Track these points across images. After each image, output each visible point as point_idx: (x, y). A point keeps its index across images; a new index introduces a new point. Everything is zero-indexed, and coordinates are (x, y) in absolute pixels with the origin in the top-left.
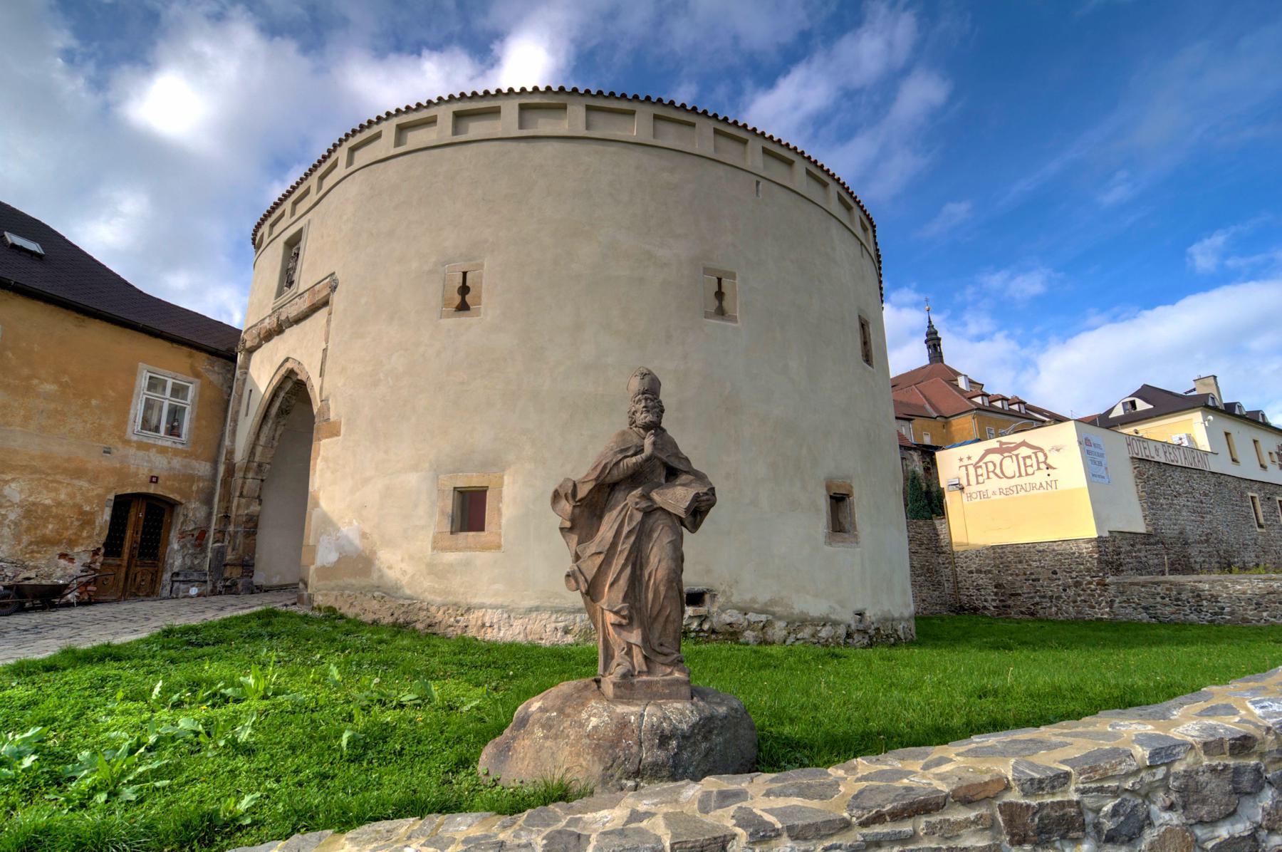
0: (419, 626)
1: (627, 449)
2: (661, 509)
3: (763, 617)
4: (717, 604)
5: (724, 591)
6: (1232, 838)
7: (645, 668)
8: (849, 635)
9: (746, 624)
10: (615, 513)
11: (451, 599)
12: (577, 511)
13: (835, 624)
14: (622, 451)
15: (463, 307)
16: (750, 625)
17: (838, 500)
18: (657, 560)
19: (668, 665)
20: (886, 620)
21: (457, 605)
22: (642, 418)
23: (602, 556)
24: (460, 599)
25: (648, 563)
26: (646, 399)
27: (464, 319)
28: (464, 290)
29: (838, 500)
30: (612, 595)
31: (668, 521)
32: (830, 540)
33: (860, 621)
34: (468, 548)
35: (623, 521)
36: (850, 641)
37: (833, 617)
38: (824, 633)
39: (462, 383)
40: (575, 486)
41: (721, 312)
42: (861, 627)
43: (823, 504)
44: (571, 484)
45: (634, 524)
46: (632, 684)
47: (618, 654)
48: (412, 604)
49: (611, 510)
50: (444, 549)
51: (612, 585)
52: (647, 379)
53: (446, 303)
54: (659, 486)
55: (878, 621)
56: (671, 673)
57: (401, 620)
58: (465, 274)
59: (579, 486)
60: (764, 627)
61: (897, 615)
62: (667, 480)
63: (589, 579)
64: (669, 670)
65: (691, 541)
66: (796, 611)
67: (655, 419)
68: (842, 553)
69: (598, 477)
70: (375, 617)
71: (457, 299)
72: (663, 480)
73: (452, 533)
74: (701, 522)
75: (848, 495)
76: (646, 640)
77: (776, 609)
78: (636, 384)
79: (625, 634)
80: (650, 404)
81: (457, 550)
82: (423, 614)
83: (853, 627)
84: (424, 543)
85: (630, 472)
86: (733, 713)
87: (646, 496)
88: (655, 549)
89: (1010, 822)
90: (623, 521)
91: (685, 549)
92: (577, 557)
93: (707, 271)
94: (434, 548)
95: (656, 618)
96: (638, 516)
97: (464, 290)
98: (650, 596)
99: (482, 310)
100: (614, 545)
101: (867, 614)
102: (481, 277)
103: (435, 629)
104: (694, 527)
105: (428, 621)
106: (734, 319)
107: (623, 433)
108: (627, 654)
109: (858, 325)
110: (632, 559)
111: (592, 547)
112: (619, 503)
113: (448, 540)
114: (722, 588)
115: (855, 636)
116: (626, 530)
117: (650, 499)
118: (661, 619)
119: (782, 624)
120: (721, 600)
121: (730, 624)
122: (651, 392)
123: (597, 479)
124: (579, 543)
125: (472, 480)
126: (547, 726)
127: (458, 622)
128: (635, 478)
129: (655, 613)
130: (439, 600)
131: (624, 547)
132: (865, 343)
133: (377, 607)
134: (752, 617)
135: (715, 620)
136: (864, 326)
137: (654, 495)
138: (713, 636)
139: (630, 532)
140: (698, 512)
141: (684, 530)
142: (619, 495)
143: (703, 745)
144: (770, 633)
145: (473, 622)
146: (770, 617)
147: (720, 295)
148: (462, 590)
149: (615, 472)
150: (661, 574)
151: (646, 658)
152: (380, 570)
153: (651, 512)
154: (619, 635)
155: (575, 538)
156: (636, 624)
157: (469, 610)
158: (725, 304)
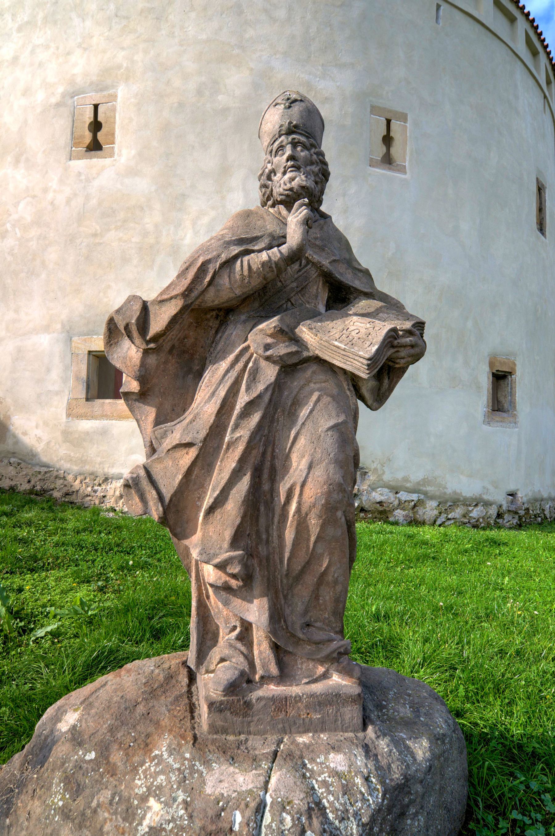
0: (56, 494)
1: (256, 239)
2: (318, 360)
3: (415, 497)
4: (367, 482)
5: (376, 469)
7: (274, 670)
8: (499, 515)
9: (396, 503)
10: (224, 365)
11: (88, 468)
12: (152, 360)
13: (487, 504)
14: (241, 241)
15: (95, 146)
16: (401, 505)
17: (500, 378)
18: (304, 464)
19: (322, 662)
20: (536, 500)
21: (94, 475)
22: (282, 183)
23: (193, 452)
24: (100, 471)
25: (286, 468)
26: (294, 144)
27: (96, 161)
28: (96, 126)
30: (211, 529)
31: (331, 385)
32: (488, 420)
33: (512, 502)
34: (104, 416)
35: (237, 383)
36: (500, 521)
37: (485, 497)
38: (476, 513)
39: (95, 235)
40: (145, 308)
41: (388, 160)
42: (513, 508)
44: (137, 308)
45: (260, 387)
46: (248, 705)
47: (226, 637)
48: (48, 472)
49: (216, 360)
51: (211, 510)
52: (296, 108)
53: (75, 141)
54: (314, 315)
55: (529, 502)
56: (325, 676)
57: (38, 488)
58: (96, 107)
59: (152, 309)
60: (415, 506)
61: (545, 495)
62: (328, 307)
63: (167, 498)
64: (321, 670)
65: (375, 430)
66: (449, 491)
67: (310, 183)
68: (501, 435)
70: (13, 483)
71: (88, 137)
72: (322, 308)
73: (87, 399)
74: (391, 389)
75: (510, 373)
76: (276, 617)
77: (428, 488)
78: (274, 119)
79: (237, 602)
80: (302, 154)
81: (93, 417)
82: (59, 482)
83: (504, 508)
84: (58, 408)
85: (256, 282)
87: (287, 334)
88: (302, 441)
90: (237, 383)
91: (361, 437)
92: (152, 450)
93: (375, 110)
94: (68, 415)
95: (299, 577)
96: (270, 373)
97: (96, 126)
98: (289, 535)
99: (116, 150)
100: (217, 429)
101: (519, 495)
102: (114, 110)
103: (73, 498)
104: (379, 398)
105: (65, 490)
106: (402, 170)
107: (247, 215)
108: (240, 638)
109: (535, 189)
110: (253, 460)
111: (177, 434)
112: (234, 346)
113: (84, 407)
114: (373, 466)
115: (506, 516)
116: (243, 399)
117: (296, 340)
118: (310, 580)
119: (434, 504)
120: (372, 478)
121: (380, 503)
122: (304, 133)
123: (186, 294)
124: (158, 422)
126: (74, 786)
127: (95, 491)
128: (269, 296)
129: (297, 568)
130: (75, 468)
131: (239, 435)
132: (541, 210)
133: (13, 473)
134: (404, 496)
135: (364, 498)
136: (540, 189)
137: (305, 332)
138: (362, 515)
139: (250, 406)
140: (390, 366)
141: (360, 404)
142: (233, 331)
144: (420, 512)
145: (111, 493)
146: (422, 497)
147: (388, 140)
148: (99, 459)
149: (224, 281)
150: (313, 492)
151: (276, 648)
152: (14, 436)
153: (296, 364)
154: (226, 603)
155: (150, 413)
156: (258, 586)
157: (106, 480)
158: (393, 151)
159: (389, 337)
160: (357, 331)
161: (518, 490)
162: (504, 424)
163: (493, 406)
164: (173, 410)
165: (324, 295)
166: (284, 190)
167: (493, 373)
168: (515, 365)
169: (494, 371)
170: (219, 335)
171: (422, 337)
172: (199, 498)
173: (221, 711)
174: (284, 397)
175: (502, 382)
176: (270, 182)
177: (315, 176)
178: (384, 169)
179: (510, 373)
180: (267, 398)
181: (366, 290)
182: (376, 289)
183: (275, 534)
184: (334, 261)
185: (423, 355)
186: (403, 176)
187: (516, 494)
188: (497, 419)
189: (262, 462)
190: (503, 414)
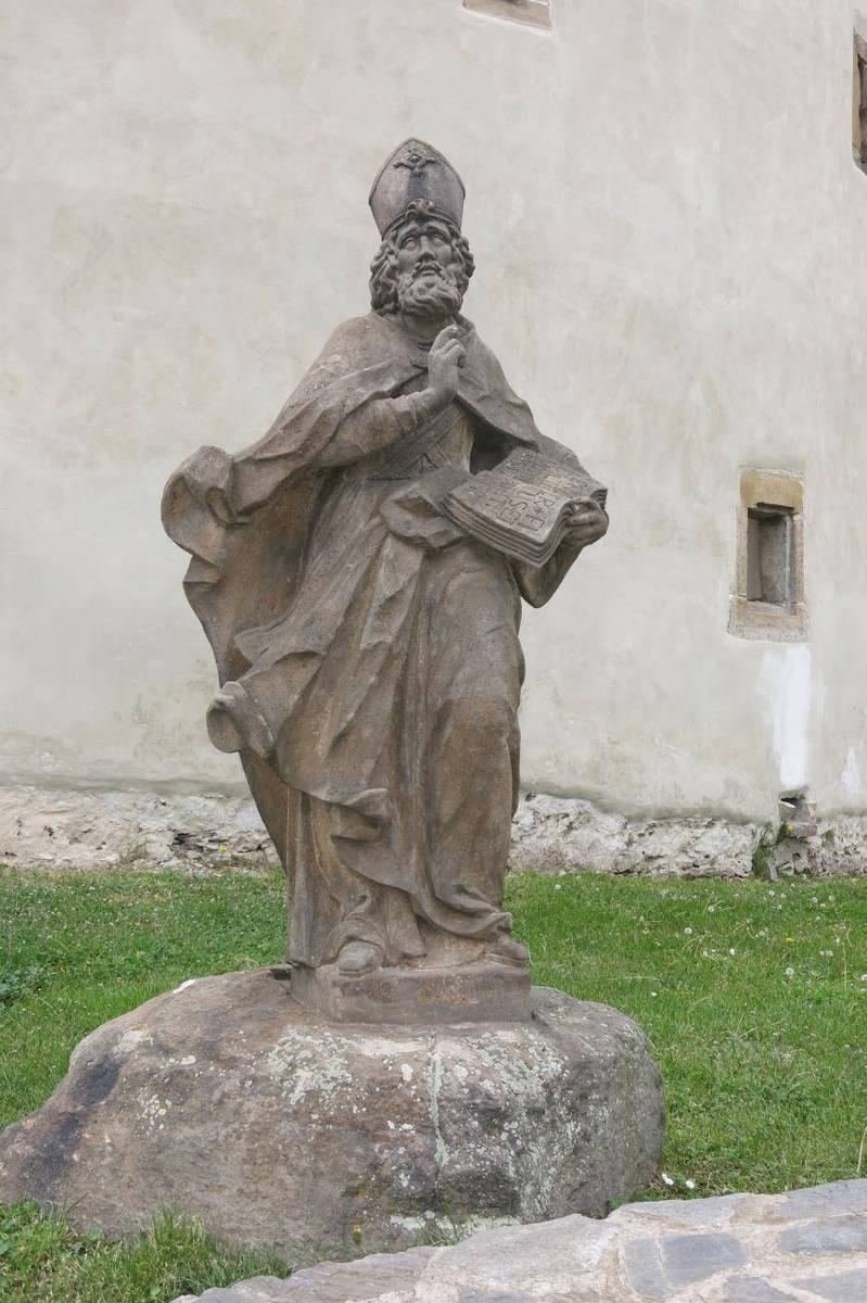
1: (378, 375)
17: (769, 522)
29: (769, 522)
43: (732, 529)
69: (305, 447)
75: (790, 511)
86: (624, 1050)
101: (810, 800)
143: (571, 1126)
159: (564, 514)
160: (524, 506)
161: (806, 788)
162: (774, 632)
163: (750, 588)
164: (258, 608)
165: (467, 447)
166: (417, 301)
167: (750, 511)
168: (801, 490)
169: (753, 506)
170: (328, 506)
171: (603, 508)
172: (317, 726)
173: (356, 994)
174: (429, 591)
175: (770, 531)
176: (393, 282)
177: (457, 278)
178: (498, 14)
179: (791, 509)
180: (410, 592)
181: (525, 438)
182: (539, 433)
183: (314, 841)
184: (483, 398)
185: (605, 533)
186: (541, 33)
187: (802, 797)
188: (759, 621)
189: (404, 676)
190: (773, 607)
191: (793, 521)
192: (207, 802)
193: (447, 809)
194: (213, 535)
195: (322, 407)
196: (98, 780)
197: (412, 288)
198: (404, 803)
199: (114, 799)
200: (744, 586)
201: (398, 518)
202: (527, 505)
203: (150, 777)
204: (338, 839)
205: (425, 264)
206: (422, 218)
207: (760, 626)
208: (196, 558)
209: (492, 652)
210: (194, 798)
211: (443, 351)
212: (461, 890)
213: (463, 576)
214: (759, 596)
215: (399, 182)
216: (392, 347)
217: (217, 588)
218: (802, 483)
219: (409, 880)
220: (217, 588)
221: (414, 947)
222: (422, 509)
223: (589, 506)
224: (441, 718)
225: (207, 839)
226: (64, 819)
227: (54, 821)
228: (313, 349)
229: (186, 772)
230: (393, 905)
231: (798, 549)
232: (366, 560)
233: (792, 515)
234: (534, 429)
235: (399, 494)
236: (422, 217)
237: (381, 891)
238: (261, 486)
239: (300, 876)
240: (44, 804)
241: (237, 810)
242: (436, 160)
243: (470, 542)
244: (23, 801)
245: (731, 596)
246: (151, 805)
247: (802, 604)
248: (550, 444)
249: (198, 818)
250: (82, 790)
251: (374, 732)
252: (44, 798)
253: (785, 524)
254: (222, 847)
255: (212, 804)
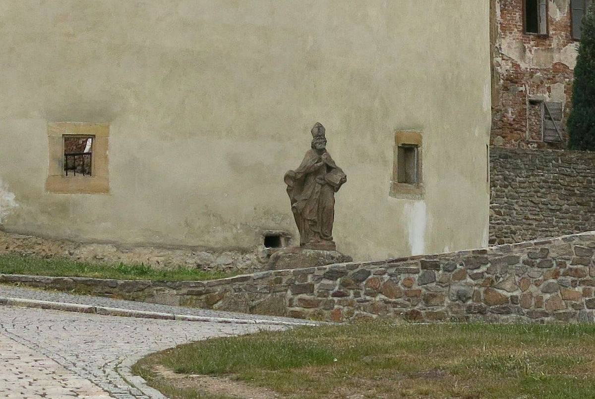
6: (477, 273)
17: (408, 152)
29: (408, 152)
32: (395, 190)
43: (391, 155)
50: (56, 191)
89: (422, 265)
125: (81, 129)
168: (421, 137)
169: (400, 145)
179: (417, 145)
190: (410, 185)
191: (418, 150)
192: (207, 254)
193: (324, 221)
194: (291, 183)
195: (308, 165)
196: (174, 246)
197: (319, 146)
198: (319, 220)
199: (178, 252)
200: (396, 177)
201: (318, 180)
202: (335, 178)
203: (190, 245)
204: (309, 225)
205: (321, 143)
206: (320, 136)
207: (403, 193)
208: (288, 185)
209: (331, 199)
210: (203, 252)
211: (323, 157)
212: (326, 233)
213: (327, 189)
214: (404, 181)
215: (316, 130)
216: (316, 155)
217: (291, 190)
218: (422, 134)
219: (320, 231)
220: (291, 190)
221: (320, 240)
222: (321, 179)
223: (344, 178)
224: (324, 208)
225: (207, 267)
226: (162, 258)
227: (160, 259)
228: (303, 156)
229: (201, 243)
230: (317, 234)
231: (420, 161)
232: (313, 187)
233: (417, 148)
234: (335, 165)
235: (318, 177)
236: (319, 134)
237: (315, 232)
238: (299, 176)
239: (303, 231)
240: (156, 253)
241: (217, 257)
242: (322, 126)
243: (327, 183)
244: (149, 252)
245: (391, 182)
246: (190, 255)
247: (422, 184)
248: (337, 167)
249: (205, 259)
250: (169, 249)
251: (315, 210)
252: (156, 252)
253: (415, 151)
254: (212, 270)
255: (209, 255)
